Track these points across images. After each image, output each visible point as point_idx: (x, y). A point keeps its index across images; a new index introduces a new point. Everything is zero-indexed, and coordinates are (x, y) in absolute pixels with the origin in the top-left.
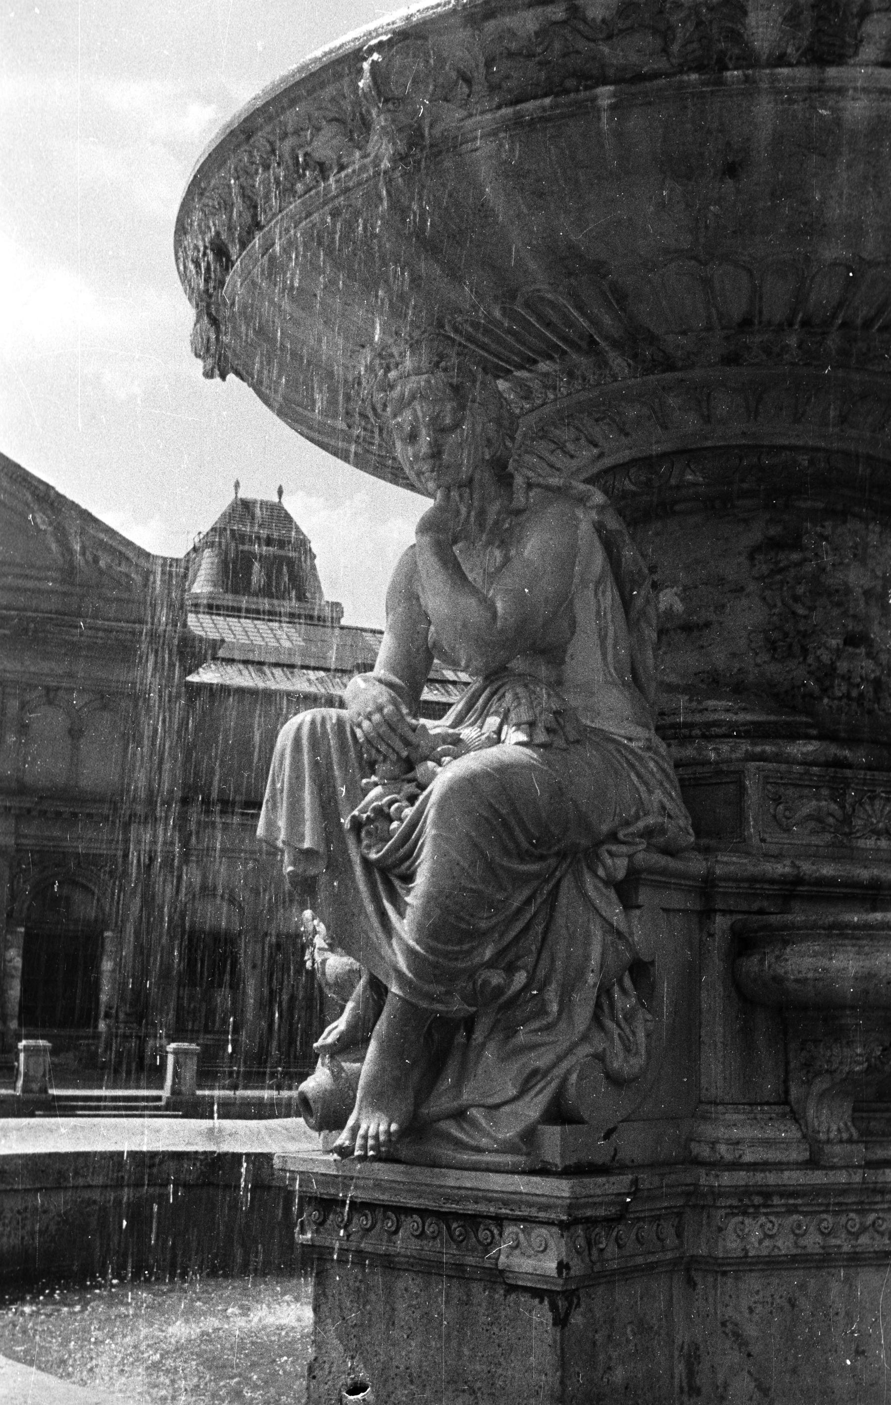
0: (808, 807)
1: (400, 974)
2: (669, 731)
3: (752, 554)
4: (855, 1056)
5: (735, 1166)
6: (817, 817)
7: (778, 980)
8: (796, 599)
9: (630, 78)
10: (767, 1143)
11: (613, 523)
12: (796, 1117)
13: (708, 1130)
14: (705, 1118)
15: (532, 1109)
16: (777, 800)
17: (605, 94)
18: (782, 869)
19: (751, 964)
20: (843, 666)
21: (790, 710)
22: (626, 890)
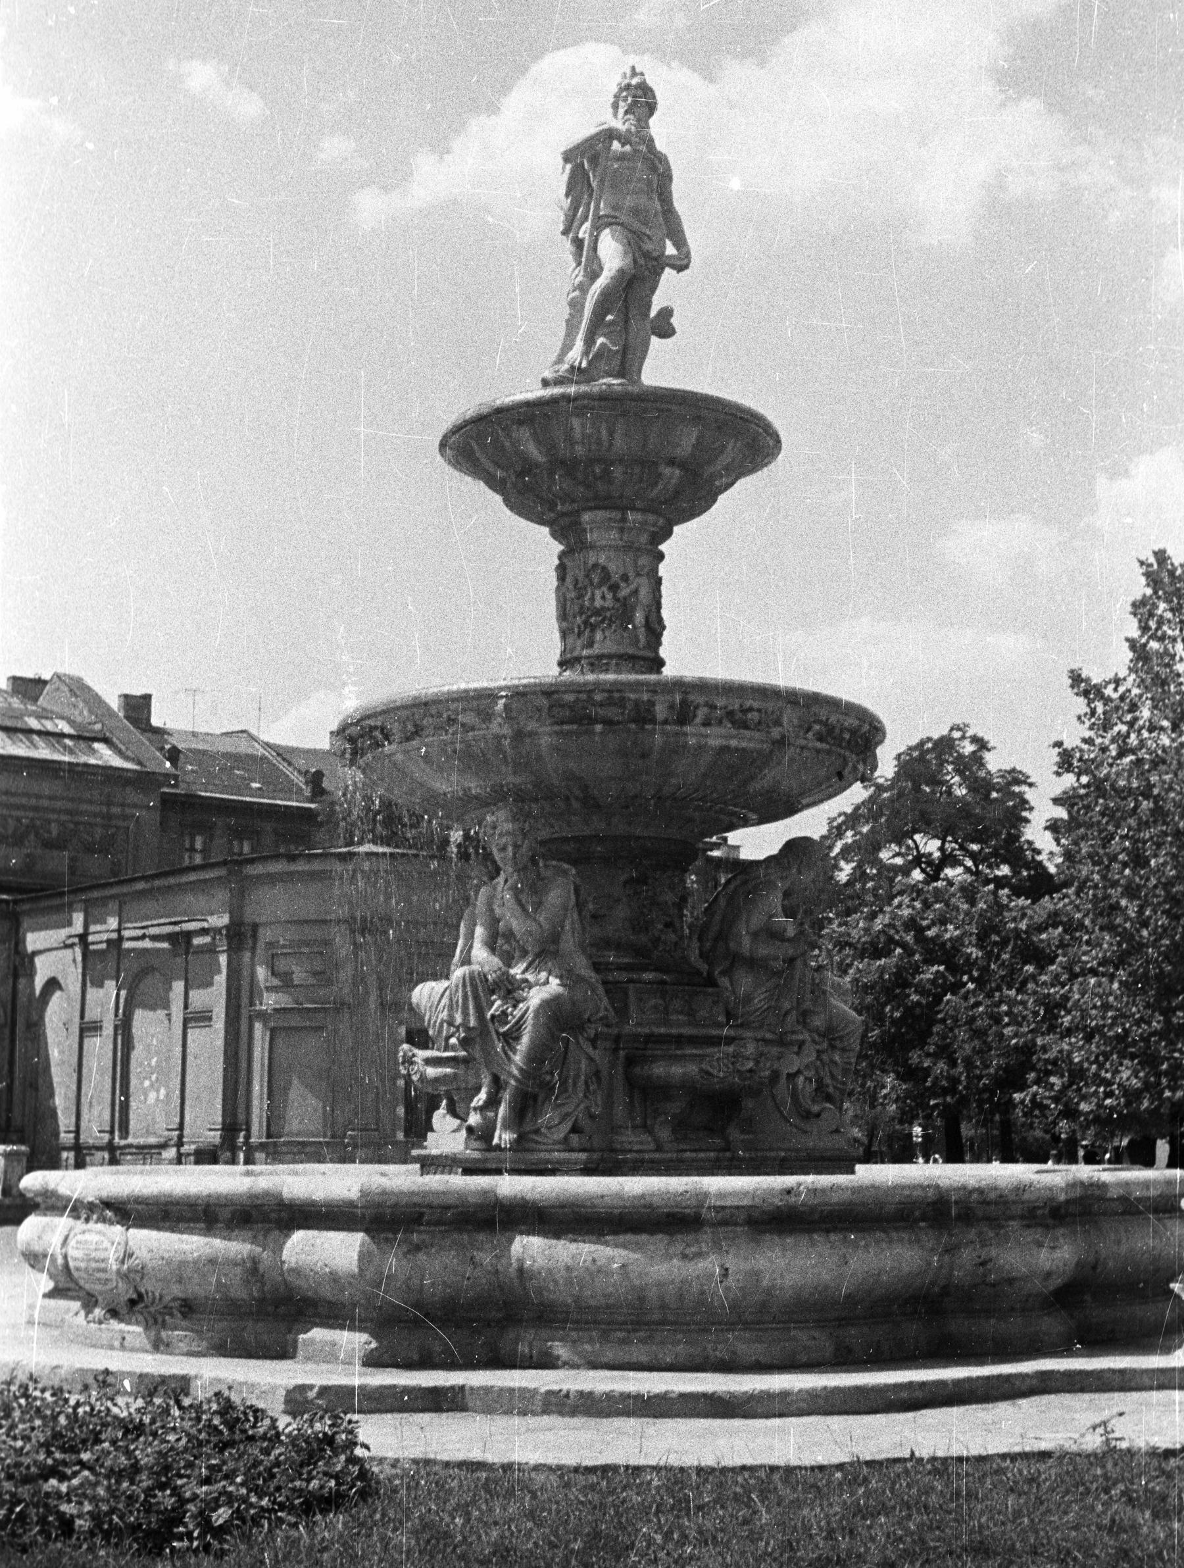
0: (652, 1002)
1: (514, 1077)
2: (597, 967)
3: (625, 883)
4: (675, 1107)
5: (631, 1151)
6: (655, 1007)
7: (649, 1077)
8: (644, 906)
9: (608, 722)
10: (641, 1143)
11: (578, 881)
12: (650, 1132)
13: (620, 1138)
14: (617, 1133)
15: (568, 1125)
16: (641, 1000)
17: (599, 728)
18: (647, 1031)
19: (637, 1070)
20: (663, 938)
21: (643, 957)
22: (593, 1042)
